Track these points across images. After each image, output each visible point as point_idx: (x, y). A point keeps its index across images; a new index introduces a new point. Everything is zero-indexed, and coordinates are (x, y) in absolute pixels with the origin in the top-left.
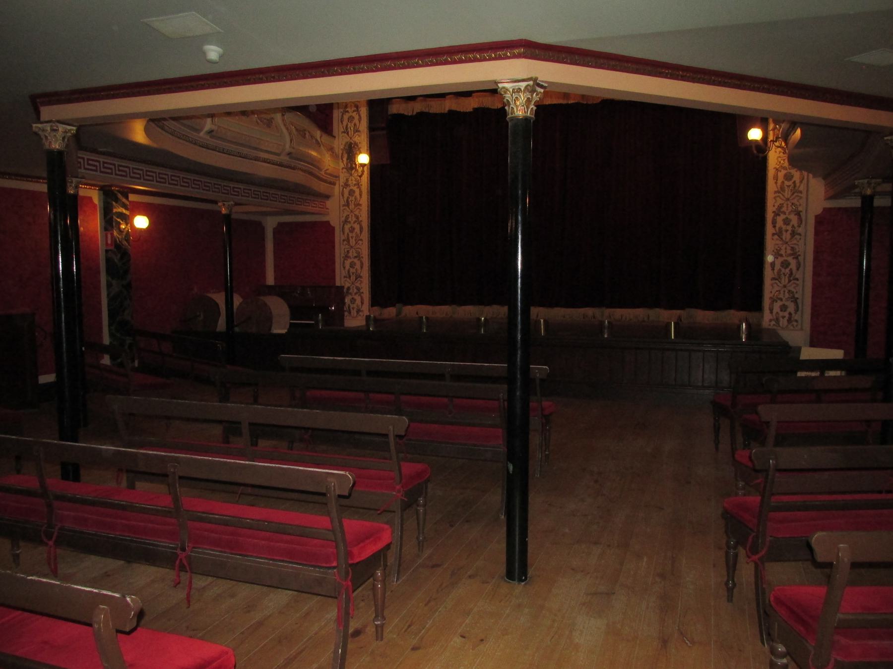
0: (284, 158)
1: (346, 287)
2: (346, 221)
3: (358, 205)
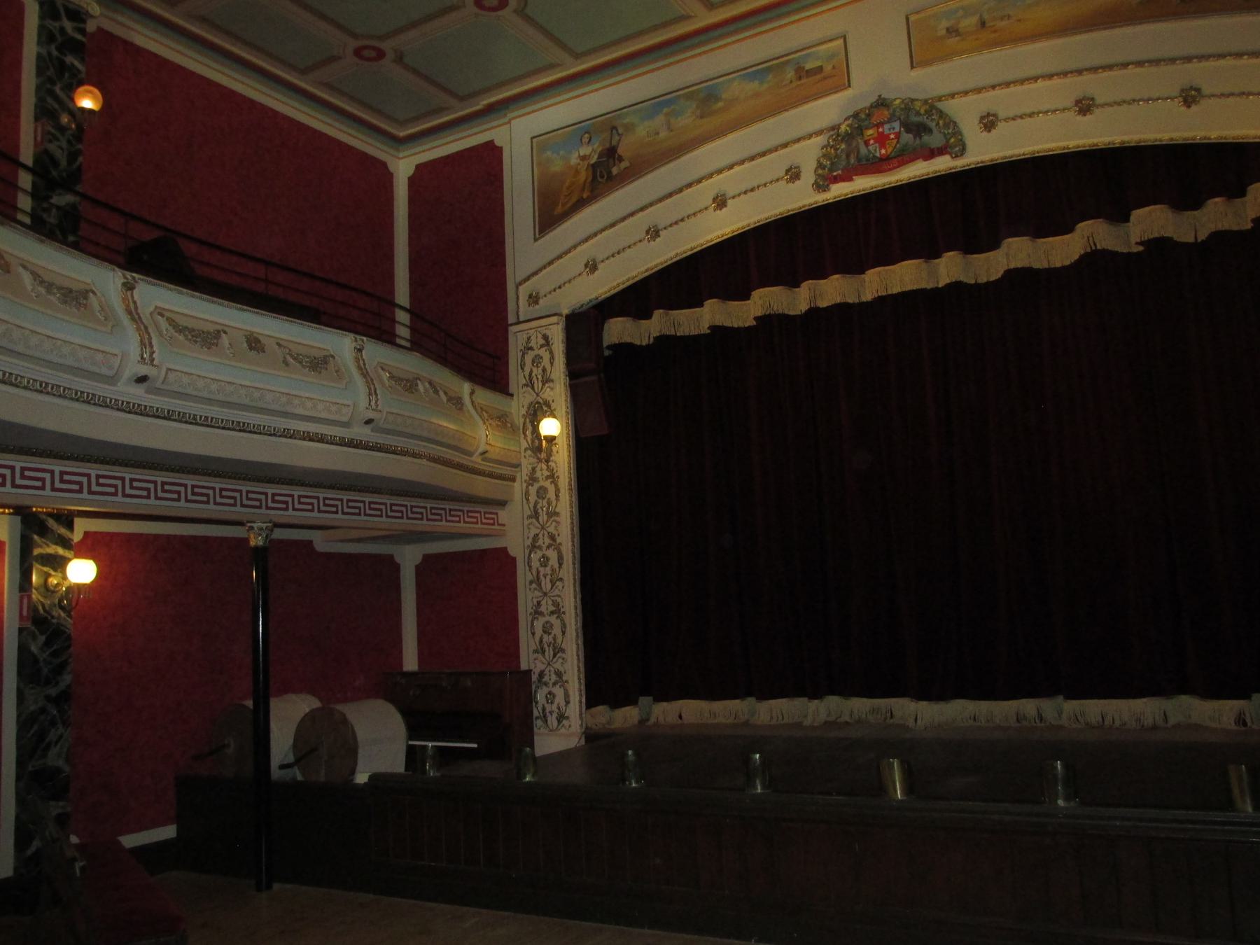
0: (360, 432)
1: (537, 671)
2: (534, 547)
3: (552, 514)
